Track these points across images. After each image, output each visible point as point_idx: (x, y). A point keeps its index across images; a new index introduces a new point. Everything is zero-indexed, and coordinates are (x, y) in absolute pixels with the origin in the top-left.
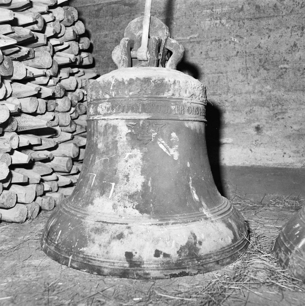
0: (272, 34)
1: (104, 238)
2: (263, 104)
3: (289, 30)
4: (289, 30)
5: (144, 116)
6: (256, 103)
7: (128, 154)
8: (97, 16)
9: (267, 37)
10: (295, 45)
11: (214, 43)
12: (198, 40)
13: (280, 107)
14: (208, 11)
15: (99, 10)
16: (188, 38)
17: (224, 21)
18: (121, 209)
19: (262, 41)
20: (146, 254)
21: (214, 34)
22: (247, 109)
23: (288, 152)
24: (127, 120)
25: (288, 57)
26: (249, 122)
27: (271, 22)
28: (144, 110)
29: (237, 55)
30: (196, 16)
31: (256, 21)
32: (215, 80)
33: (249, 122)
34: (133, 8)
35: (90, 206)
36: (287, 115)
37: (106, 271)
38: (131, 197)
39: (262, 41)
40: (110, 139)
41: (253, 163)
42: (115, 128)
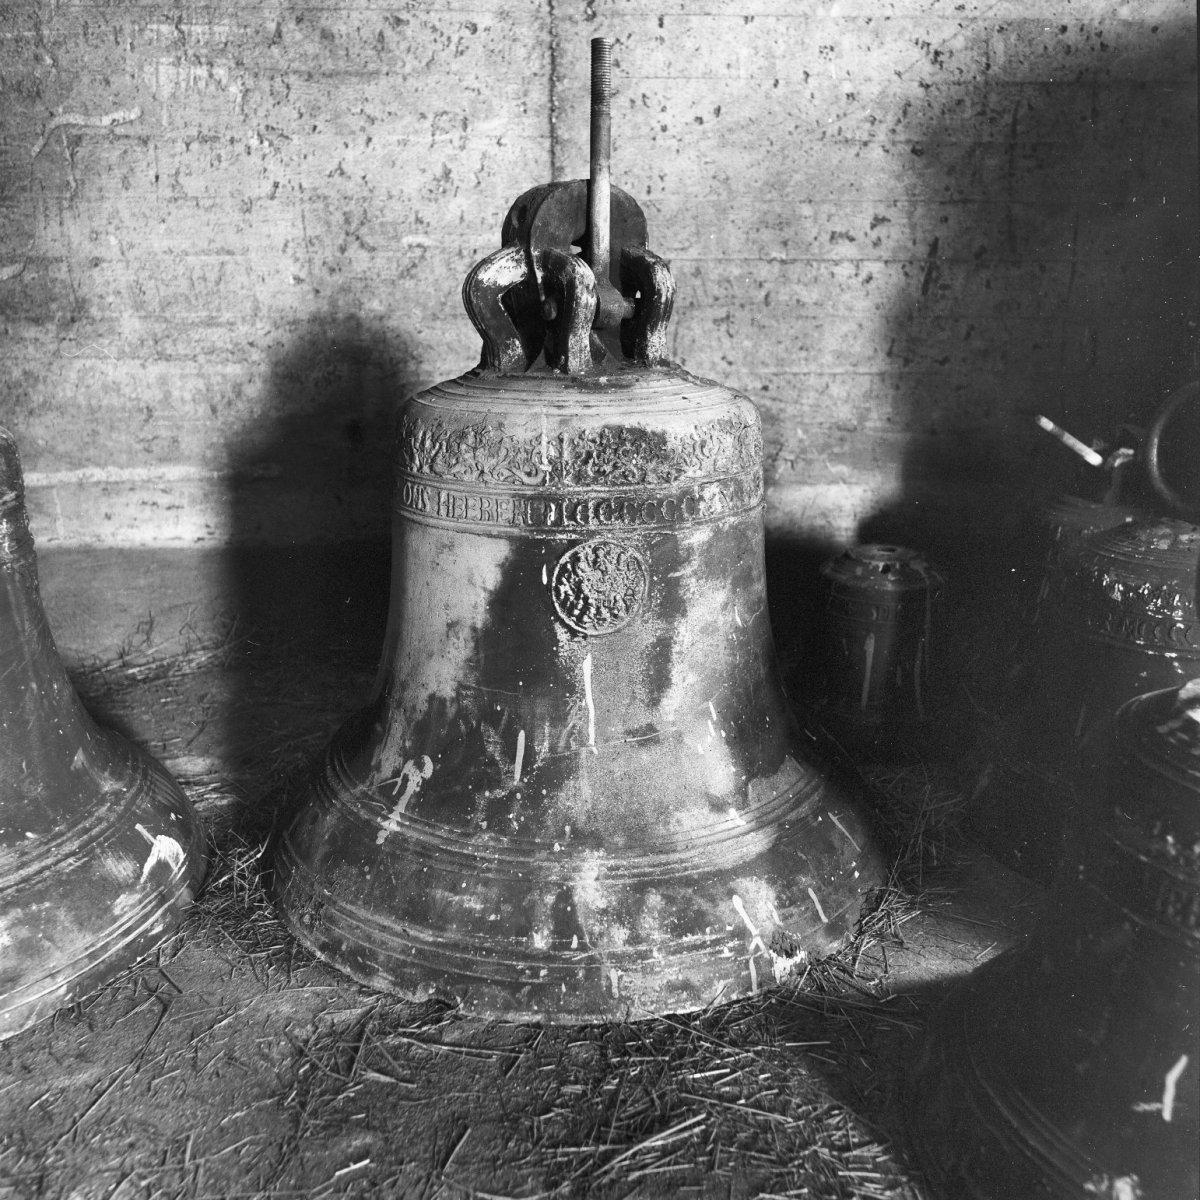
3: (427, 124)
4: (427, 124)
9: (362, 139)
10: (447, 173)
12: (144, 131)
14: (165, 28)
16: (106, 121)
17: (220, 72)
25: (428, 213)
32: (212, 276)
39: (350, 155)
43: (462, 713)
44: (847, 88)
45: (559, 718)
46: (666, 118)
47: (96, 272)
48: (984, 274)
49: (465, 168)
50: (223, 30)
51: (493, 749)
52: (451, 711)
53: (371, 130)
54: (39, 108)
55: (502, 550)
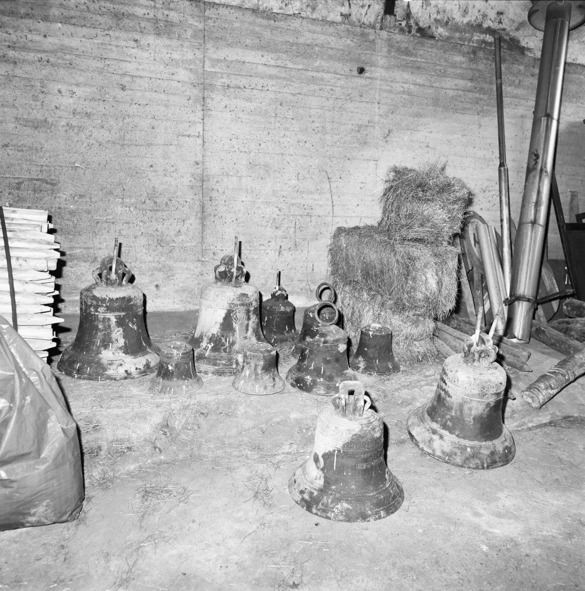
0: (165, 223)
1: (114, 367)
2: (160, 270)
3: (176, 221)
4: (176, 221)
5: (123, 314)
6: (156, 269)
7: (116, 330)
8: (18, 189)
9: (162, 224)
10: (180, 231)
11: (125, 224)
12: (113, 221)
13: (171, 272)
14: (120, 200)
15: (19, 184)
16: (105, 219)
17: (132, 209)
18: (117, 354)
19: (159, 227)
20: (132, 370)
21: (125, 218)
22: (150, 273)
23: (176, 301)
24: (115, 316)
25: (175, 239)
26: (151, 282)
27: (164, 214)
28: (123, 311)
29: (142, 235)
30: (111, 202)
31: (154, 212)
32: (127, 252)
33: (151, 282)
34: (55, 188)
35: (100, 355)
36: (175, 277)
37: (118, 379)
38: (120, 348)
39: (159, 227)
40: (107, 324)
41: (155, 310)
42: (109, 319)
43: (218, 336)
44: (263, 215)
45: (233, 336)
46: (226, 221)
47: (100, 251)
48: (291, 252)
49: (184, 229)
50: (133, 200)
51: (223, 341)
52: (216, 336)
53: (164, 222)
54: (90, 215)
55: (225, 311)
